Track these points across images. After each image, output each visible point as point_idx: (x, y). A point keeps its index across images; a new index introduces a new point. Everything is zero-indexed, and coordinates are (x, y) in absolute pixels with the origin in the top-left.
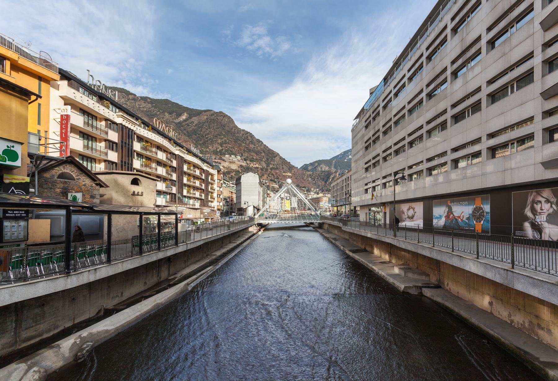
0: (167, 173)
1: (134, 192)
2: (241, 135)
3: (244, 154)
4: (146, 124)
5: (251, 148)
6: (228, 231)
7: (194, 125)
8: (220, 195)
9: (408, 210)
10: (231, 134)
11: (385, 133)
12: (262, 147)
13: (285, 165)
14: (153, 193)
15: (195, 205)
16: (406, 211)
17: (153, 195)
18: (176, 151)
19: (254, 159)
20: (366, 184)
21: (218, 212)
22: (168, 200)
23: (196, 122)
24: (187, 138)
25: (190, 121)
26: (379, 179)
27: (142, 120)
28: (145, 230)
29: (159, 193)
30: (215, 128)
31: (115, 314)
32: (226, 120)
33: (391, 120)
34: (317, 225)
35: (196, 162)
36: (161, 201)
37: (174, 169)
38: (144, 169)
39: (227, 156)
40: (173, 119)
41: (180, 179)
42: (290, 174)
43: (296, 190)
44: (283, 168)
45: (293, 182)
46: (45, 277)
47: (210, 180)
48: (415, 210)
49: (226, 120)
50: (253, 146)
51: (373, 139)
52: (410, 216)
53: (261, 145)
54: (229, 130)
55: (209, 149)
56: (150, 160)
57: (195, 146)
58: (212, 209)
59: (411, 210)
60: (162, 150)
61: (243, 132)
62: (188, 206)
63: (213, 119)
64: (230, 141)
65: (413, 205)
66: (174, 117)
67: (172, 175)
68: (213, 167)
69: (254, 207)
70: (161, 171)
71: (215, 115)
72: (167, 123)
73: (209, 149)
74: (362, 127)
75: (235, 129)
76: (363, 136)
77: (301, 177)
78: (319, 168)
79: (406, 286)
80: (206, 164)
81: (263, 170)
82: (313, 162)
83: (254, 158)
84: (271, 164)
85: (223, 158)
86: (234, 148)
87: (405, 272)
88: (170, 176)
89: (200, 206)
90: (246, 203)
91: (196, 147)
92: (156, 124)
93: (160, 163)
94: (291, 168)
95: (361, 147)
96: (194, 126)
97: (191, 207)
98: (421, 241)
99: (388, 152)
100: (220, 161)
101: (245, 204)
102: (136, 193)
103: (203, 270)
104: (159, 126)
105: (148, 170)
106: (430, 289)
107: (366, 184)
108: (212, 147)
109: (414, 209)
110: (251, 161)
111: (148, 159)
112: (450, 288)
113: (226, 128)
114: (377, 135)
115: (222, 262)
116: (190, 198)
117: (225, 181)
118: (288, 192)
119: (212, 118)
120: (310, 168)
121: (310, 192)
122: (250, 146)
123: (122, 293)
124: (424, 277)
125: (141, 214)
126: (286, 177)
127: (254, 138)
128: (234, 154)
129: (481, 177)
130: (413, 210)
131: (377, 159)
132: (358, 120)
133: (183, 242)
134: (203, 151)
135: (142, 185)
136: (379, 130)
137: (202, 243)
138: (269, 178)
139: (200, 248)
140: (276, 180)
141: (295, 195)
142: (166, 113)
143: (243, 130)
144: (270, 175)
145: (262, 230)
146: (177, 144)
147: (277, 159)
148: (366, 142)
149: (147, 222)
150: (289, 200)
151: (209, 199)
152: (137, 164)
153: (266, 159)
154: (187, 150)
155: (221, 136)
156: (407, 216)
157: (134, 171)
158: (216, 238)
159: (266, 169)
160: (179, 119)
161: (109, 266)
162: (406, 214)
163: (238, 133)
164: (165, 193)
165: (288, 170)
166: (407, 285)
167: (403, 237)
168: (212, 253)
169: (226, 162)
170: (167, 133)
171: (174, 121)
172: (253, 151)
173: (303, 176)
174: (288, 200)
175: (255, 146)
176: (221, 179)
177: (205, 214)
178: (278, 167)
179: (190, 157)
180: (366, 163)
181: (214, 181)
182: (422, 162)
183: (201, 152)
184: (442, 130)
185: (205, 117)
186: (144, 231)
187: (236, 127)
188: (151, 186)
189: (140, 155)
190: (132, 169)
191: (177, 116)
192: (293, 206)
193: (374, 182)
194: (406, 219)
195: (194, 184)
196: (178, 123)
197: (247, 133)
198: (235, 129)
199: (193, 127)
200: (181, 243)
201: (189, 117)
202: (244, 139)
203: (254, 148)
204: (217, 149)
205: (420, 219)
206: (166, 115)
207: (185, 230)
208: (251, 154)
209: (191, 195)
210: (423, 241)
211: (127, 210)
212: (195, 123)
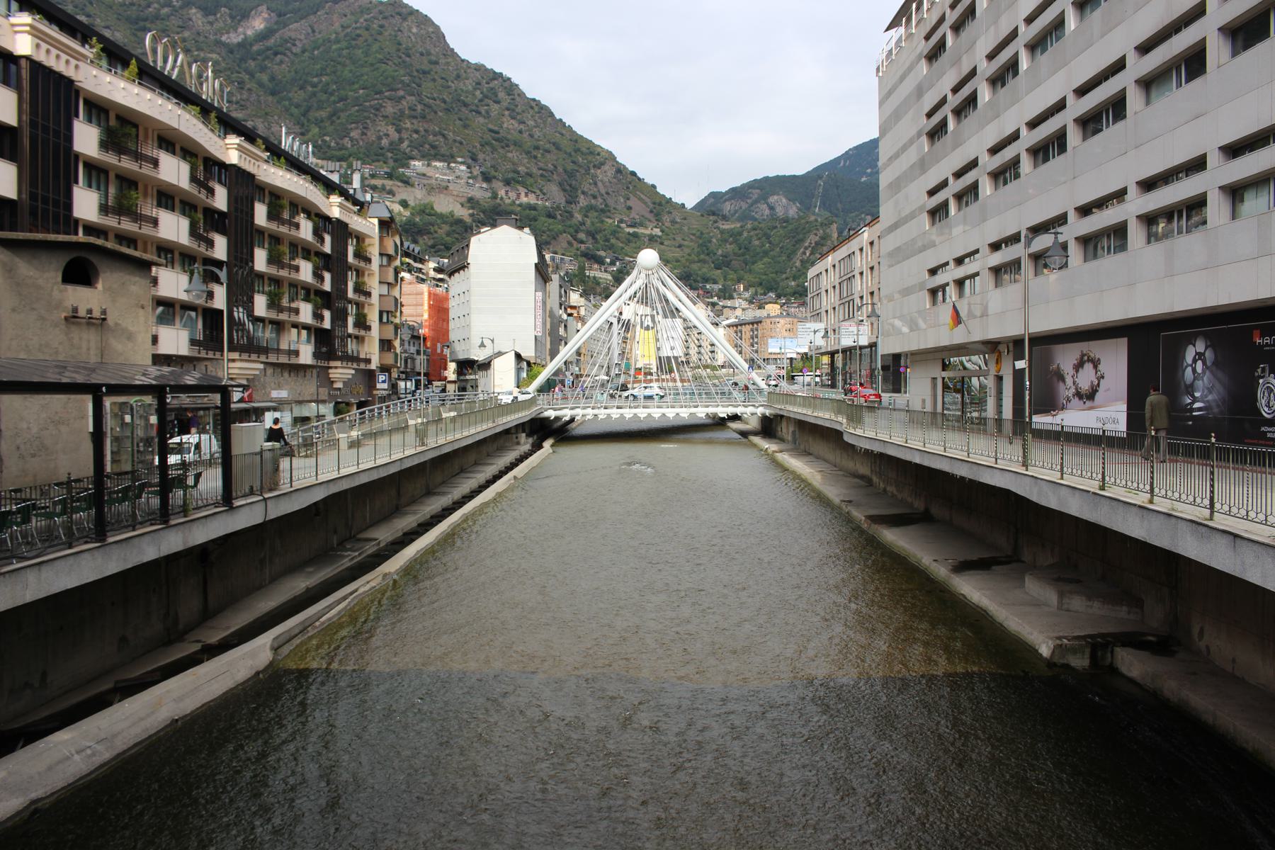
0: (193, 232)
1: (75, 310)
2: (469, 85)
4: (116, 57)
6: (420, 449)
9: (1079, 366)
10: (434, 80)
11: (998, 80)
13: (635, 195)
14: (141, 312)
15: (297, 353)
16: (1072, 372)
17: (142, 319)
18: (230, 150)
19: (518, 173)
20: (933, 272)
21: (382, 378)
22: (200, 336)
26: (977, 251)
27: (102, 39)
28: (115, 449)
29: (169, 309)
31: (22, 747)
32: (414, 30)
33: (1014, 34)
34: (754, 424)
35: (301, 192)
36: (175, 340)
38: (111, 222)
41: (240, 254)
42: (657, 232)
43: (676, 293)
45: (665, 260)
46: (17, 562)
47: (351, 259)
48: (1100, 367)
51: (954, 101)
52: (1083, 392)
55: (352, 139)
56: (133, 187)
57: (297, 129)
58: (362, 366)
59: (1088, 367)
61: (478, 74)
62: (272, 358)
64: (429, 107)
65: (1096, 348)
66: (221, 24)
67: (211, 244)
69: (518, 357)
70: (174, 228)
72: (193, 51)
73: (352, 139)
74: (913, 56)
76: (920, 91)
81: (554, 217)
82: (743, 186)
83: (521, 169)
86: (444, 136)
88: (203, 246)
89: (316, 355)
90: (487, 342)
91: (303, 134)
92: (155, 51)
93: (167, 198)
94: (660, 206)
95: (913, 132)
97: (283, 359)
98: (1113, 480)
100: (390, 183)
101: (482, 345)
102: (82, 313)
103: (328, 594)
104: (165, 61)
105: (128, 226)
106: (1143, 654)
107: (933, 272)
109: (1096, 363)
110: (507, 183)
111: (128, 183)
112: (1207, 647)
114: (965, 92)
117: (407, 260)
118: (643, 297)
121: (731, 298)
122: (505, 125)
123: (44, 675)
124: (1125, 608)
125: (96, 392)
126: (637, 243)
127: (522, 94)
128: (443, 156)
130: (1095, 367)
131: (1007, 154)
132: (901, 30)
133: (252, 493)
134: (329, 147)
136: (973, 73)
137: (319, 495)
138: (575, 244)
139: (317, 514)
140: (602, 253)
141: (673, 312)
142: (194, 11)
145: (547, 444)
146: (228, 125)
147: (609, 171)
148: (930, 115)
149: (123, 419)
150: (650, 331)
151: (351, 329)
152: (86, 204)
154: (267, 149)
155: (396, 90)
156: (1073, 390)
157: (77, 234)
158: (375, 476)
160: (240, 30)
161: (101, 550)
162: (1069, 381)
165: (651, 216)
167: (1052, 469)
169: (412, 186)
170: (191, 85)
174: (647, 328)
175: (522, 126)
177: (336, 386)
179: (281, 173)
180: (932, 193)
181: (369, 260)
182: (947, 264)
183: (321, 152)
184: (1191, 77)
186: (112, 453)
189: (97, 173)
190: (72, 224)
191: (232, 18)
192: (666, 352)
193: (959, 261)
194: (1069, 400)
196: (239, 45)
200: (245, 496)
201: (276, 23)
202: (481, 101)
203: (520, 132)
204: (380, 138)
205: (1117, 400)
207: (258, 450)
208: (510, 155)
210: (1118, 481)
211: (52, 377)
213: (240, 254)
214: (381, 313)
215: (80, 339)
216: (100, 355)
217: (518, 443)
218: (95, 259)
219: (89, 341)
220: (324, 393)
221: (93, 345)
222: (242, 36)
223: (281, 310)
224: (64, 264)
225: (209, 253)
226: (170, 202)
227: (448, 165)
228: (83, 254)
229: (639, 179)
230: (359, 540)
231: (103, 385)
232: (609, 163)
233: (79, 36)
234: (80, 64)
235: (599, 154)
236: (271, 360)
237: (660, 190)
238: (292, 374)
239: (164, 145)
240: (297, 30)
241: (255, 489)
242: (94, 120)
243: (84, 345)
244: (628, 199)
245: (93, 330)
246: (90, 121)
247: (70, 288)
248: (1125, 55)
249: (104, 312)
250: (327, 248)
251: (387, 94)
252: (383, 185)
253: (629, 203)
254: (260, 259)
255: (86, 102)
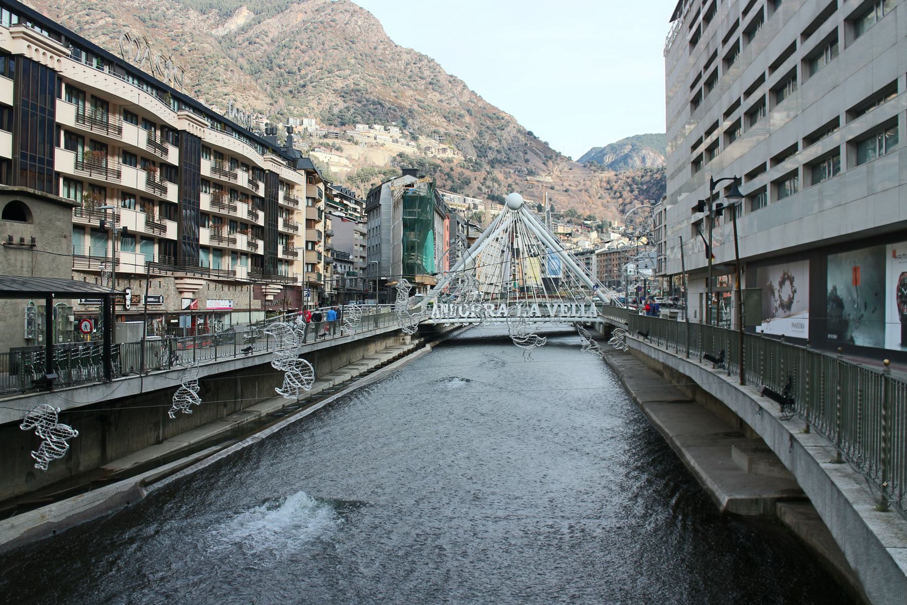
0: (150, 182)
1: (11, 238)
3: (410, 121)
5: (432, 102)
7: (268, 40)
8: (314, 243)
9: (782, 284)
12: (465, 99)
23: (274, 33)
24: (248, 77)
25: (257, 29)
30: (326, 47)
32: (359, 23)
37: (170, 172)
39: (360, 127)
40: (211, 27)
44: (527, 161)
47: (281, 201)
48: (795, 284)
49: (359, 23)
50: (438, 95)
52: (785, 303)
53: (461, 93)
54: (367, 51)
60: (140, 120)
63: (322, 22)
68: (293, 162)
71: (329, 11)
75: (385, 49)
77: (580, 187)
78: (636, 158)
79: (732, 497)
80: (269, 155)
84: (490, 148)
85: (350, 133)
87: (751, 462)
93: (131, 156)
96: (267, 44)
99: (788, 165)
102: (16, 240)
108: (319, 104)
109: (792, 280)
111: (102, 147)
113: (360, 46)
114: (712, 68)
115: (274, 427)
116: (219, 252)
119: (320, 17)
120: (608, 159)
122: (429, 96)
125: (47, 296)
129: (897, 188)
130: (791, 284)
135: (32, 220)
143: (409, 52)
144: (489, 183)
149: (68, 319)
153: (475, 133)
159: (476, 163)
160: (226, 25)
163: (393, 59)
164: (147, 239)
166: (738, 497)
168: (250, 406)
169: (356, 143)
171: (214, 32)
172: (436, 110)
173: (588, 182)
176: (317, 197)
178: (513, 157)
185: (301, 17)
187: (389, 42)
188: (58, 223)
189: (74, 139)
194: (777, 310)
195: (232, 214)
197: (421, 58)
198: (385, 49)
199: (266, 47)
201: (254, 20)
202: (410, 77)
203: (441, 101)
205: (803, 310)
206: (192, 17)
209: (224, 245)
211: (16, 287)
212: (271, 36)
213: (189, 197)
214: (307, 242)
215: (16, 260)
216: (31, 271)
217: (404, 344)
218: (27, 202)
219: (22, 261)
220: (257, 304)
221: (25, 265)
222: (228, 30)
223: (221, 239)
224: (4, 206)
225: (163, 197)
226: (133, 160)
227: (385, 127)
228: (18, 199)
229: (535, 138)
230: (245, 412)
231: (53, 292)
232: (512, 125)
233: (63, 38)
234: (62, 59)
235: (503, 119)
236: (212, 278)
237: (551, 146)
238: (231, 288)
239: (129, 116)
240: (273, 26)
241: (134, 369)
242: (74, 100)
243: (19, 264)
244: (526, 154)
245: (26, 253)
246: (70, 101)
247: (8, 223)
248: (796, 40)
249: (33, 240)
250: (261, 193)
251: (337, 73)
252: (334, 143)
253: (527, 157)
254: (205, 202)
255: (67, 86)
